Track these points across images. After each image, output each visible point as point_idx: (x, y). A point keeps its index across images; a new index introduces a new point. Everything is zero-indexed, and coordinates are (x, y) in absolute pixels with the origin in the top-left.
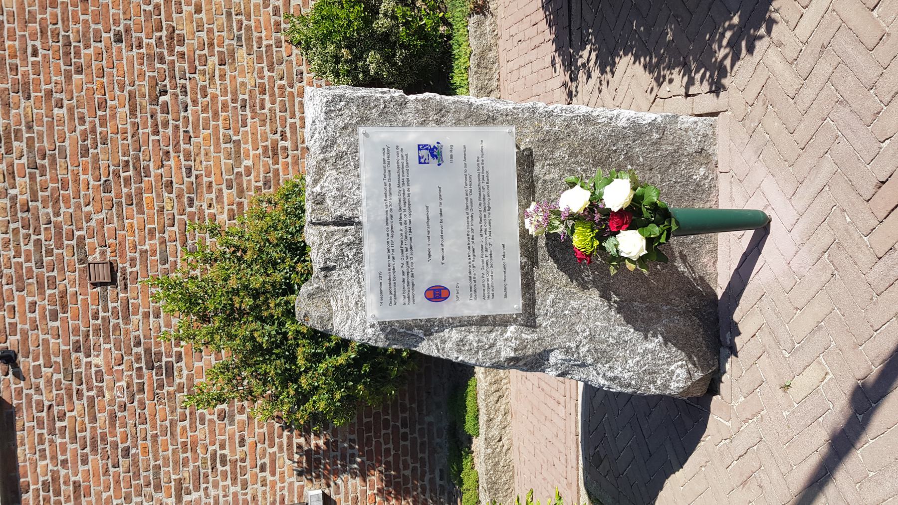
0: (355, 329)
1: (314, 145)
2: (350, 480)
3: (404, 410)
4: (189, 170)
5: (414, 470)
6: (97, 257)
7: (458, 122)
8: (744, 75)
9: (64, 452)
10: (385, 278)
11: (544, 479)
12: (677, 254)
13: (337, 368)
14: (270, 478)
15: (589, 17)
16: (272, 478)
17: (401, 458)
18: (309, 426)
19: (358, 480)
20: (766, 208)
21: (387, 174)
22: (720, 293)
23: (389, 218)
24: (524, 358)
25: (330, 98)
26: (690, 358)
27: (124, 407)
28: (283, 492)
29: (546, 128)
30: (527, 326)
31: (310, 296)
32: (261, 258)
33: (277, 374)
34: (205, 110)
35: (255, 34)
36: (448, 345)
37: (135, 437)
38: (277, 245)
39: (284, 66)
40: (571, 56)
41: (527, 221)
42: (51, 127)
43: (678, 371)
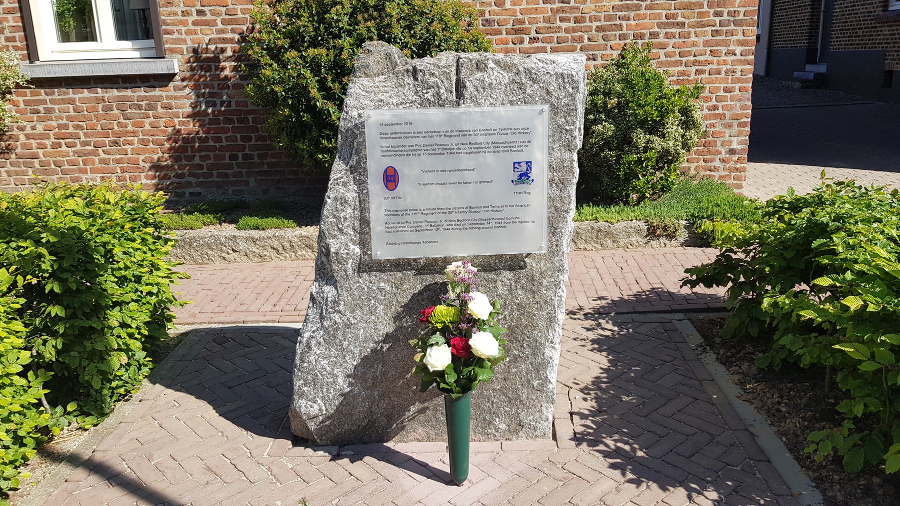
0: (357, 99)
1: (533, 62)
2: (189, 102)
3: (262, 157)
5: (200, 166)
7: (551, 199)
8: (591, 460)
10: (406, 129)
11: (197, 292)
12: (426, 404)
13: (306, 88)
14: (190, 19)
15: (644, 329)
16: (190, 22)
17: (212, 154)
18: (244, 60)
19: (189, 110)
20: (470, 481)
21: (503, 131)
22: (390, 444)
23: (462, 133)
24: (329, 261)
25: (576, 78)
26: (329, 418)
28: (176, 33)
29: (545, 282)
30: (360, 264)
31: (388, 56)
32: (415, 14)
33: (299, 27)
35: (632, 14)
36: (341, 189)
38: (428, 31)
39: (601, 42)
40: (608, 314)
41: (460, 263)
43: (316, 406)
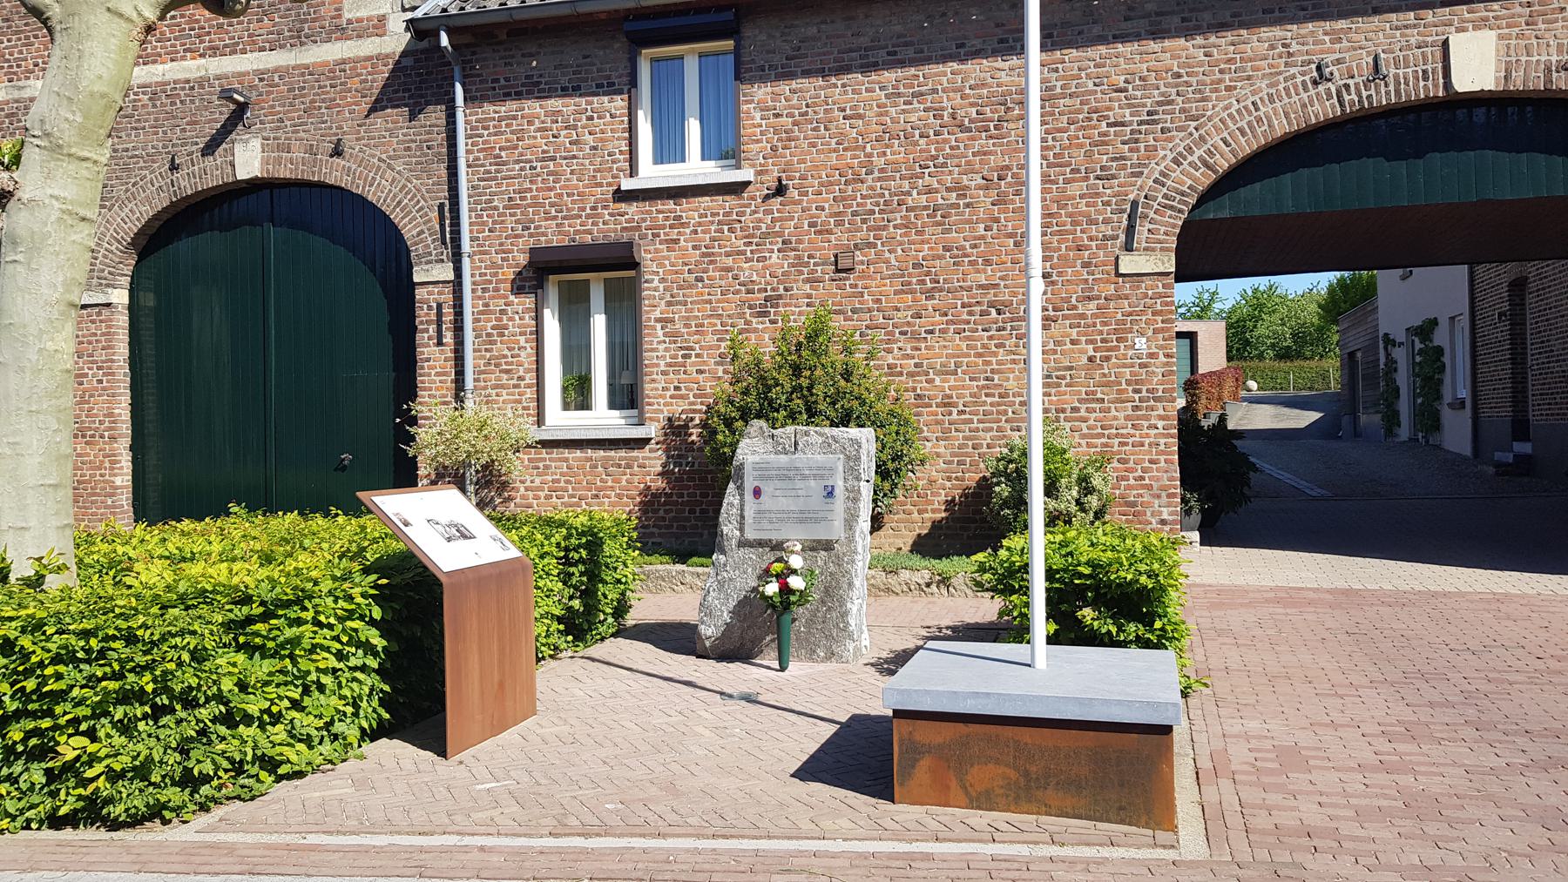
4: (931, 332)
5: (664, 519)
6: (859, 256)
9: (704, 232)
21: (819, 468)
23: (797, 469)
27: (736, 278)
34: (983, 346)
37: (711, 286)
42: (969, 222)
